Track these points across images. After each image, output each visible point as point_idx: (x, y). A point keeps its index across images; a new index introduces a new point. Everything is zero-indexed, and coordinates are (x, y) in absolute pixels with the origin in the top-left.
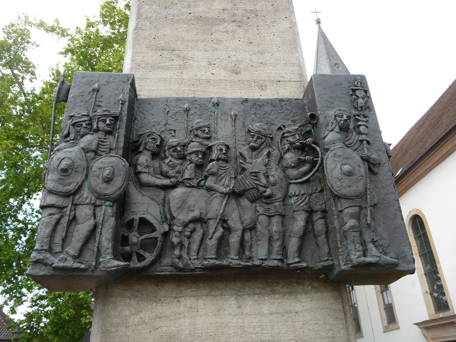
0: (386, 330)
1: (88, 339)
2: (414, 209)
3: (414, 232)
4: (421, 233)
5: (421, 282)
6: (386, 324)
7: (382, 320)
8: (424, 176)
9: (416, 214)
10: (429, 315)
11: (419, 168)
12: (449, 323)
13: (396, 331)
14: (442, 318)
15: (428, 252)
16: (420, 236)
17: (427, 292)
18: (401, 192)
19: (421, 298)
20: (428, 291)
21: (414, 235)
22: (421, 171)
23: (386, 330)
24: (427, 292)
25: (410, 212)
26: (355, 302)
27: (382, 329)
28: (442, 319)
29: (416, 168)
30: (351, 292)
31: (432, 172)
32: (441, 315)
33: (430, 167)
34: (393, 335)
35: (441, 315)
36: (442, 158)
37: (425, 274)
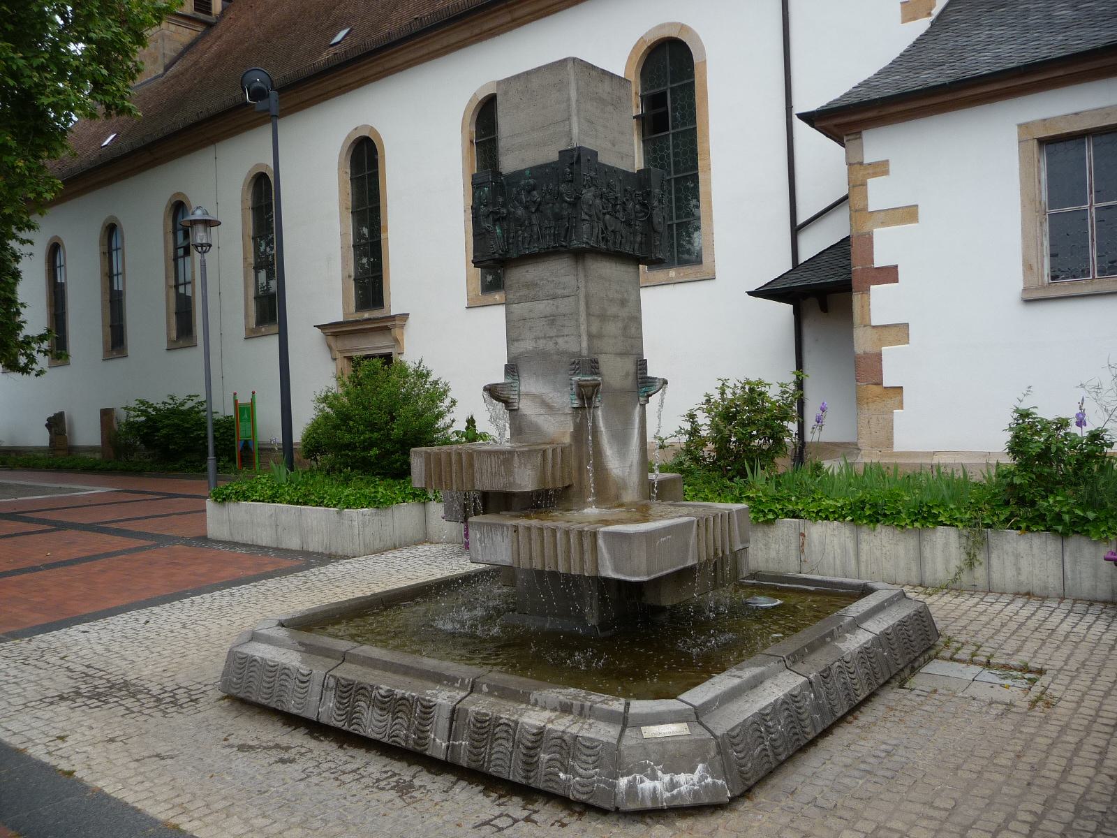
0: (173, 346)
1: (2, 470)
2: (366, 126)
3: (351, 169)
4: (367, 172)
5: (343, 257)
6: (174, 335)
7: (246, 316)
8: (401, 70)
9: (367, 135)
10: (345, 314)
11: (399, 53)
12: (377, 327)
13: (193, 348)
14: (369, 320)
15: (371, 210)
16: (363, 178)
17: (350, 276)
18: (350, 84)
19: (338, 285)
20: (353, 274)
21: (352, 174)
22: (400, 58)
23: (173, 346)
24: (350, 276)
25: (356, 129)
26: (120, 271)
27: (164, 344)
28: (368, 320)
29: (418, 40)
30: (181, 261)
31: (543, 19)
32: (366, 315)
33: (417, 58)
34: (118, 365)
35: (366, 315)
36: (511, 24)
37: (353, 246)
